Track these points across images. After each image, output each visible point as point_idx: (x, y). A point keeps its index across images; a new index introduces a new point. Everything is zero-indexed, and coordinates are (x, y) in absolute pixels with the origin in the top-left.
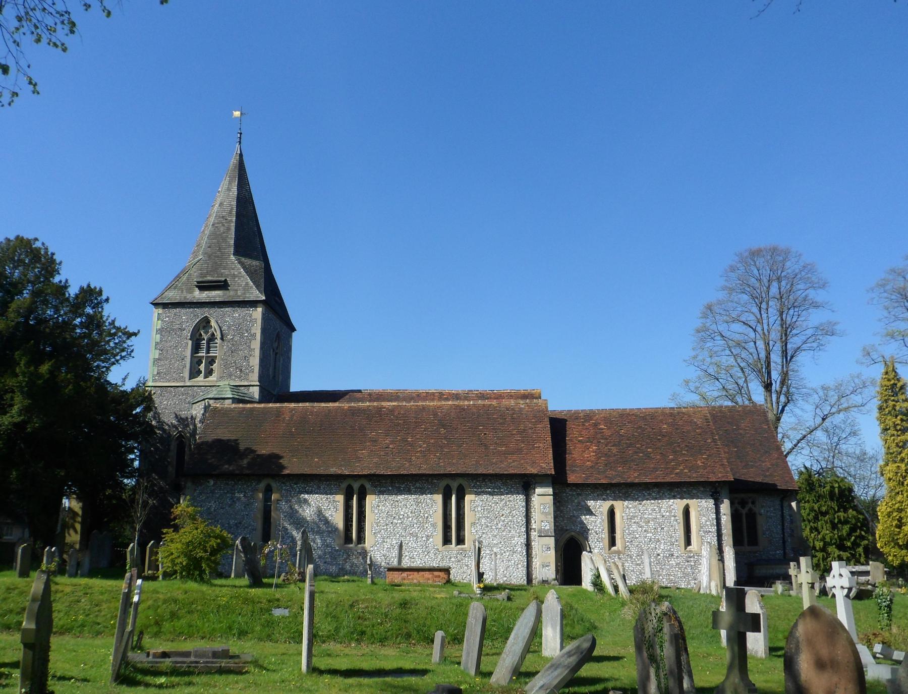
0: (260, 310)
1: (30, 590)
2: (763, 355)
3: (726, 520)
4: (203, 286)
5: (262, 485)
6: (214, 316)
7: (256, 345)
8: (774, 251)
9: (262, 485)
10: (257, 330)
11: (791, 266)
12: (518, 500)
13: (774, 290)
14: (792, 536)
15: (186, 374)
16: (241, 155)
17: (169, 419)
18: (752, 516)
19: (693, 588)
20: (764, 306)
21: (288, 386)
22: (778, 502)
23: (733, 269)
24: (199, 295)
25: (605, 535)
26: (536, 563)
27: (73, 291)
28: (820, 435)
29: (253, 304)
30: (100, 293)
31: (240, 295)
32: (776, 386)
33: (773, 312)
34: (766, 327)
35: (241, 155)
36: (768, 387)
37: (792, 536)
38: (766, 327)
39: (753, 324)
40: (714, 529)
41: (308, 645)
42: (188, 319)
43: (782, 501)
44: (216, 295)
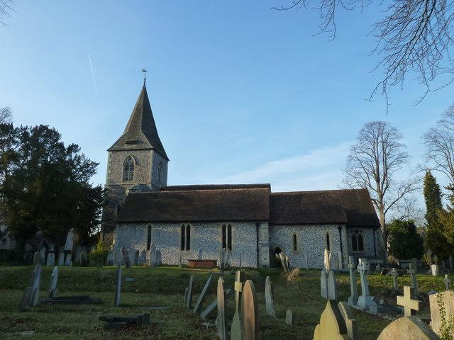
0: (152, 151)
1: (323, 264)
2: (375, 167)
3: (344, 239)
4: (129, 143)
5: (181, 225)
6: (134, 153)
7: (150, 167)
8: (380, 123)
9: (147, 226)
10: (150, 161)
11: (387, 129)
12: (252, 228)
13: (380, 139)
14: (378, 246)
15: (121, 180)
16: (144, 89)
17: (391, 223)
18: (361, 238)
19: (115, 275)
20: (376, 146)
21: (166, 184)
22: (372, 232)
23: (363, 130)
24: (126, 147)
25: (292, 246)
26: (262, 258)
27: (66, 146)
28: (402, 201)
29: (149, 149)
30: (77, 146)
31: (143, 146)
32: (381, 180)
33: (380, 148)
34: (376, 154)
35: (144, 89)
36: (378, 181)
37: (378, 246)
38: (376, 154)
39: (371, 153)
40: (339, 243)
41: (70, 298)
42: (122, 157)
43: (374, 231)
44: (134, 146)
